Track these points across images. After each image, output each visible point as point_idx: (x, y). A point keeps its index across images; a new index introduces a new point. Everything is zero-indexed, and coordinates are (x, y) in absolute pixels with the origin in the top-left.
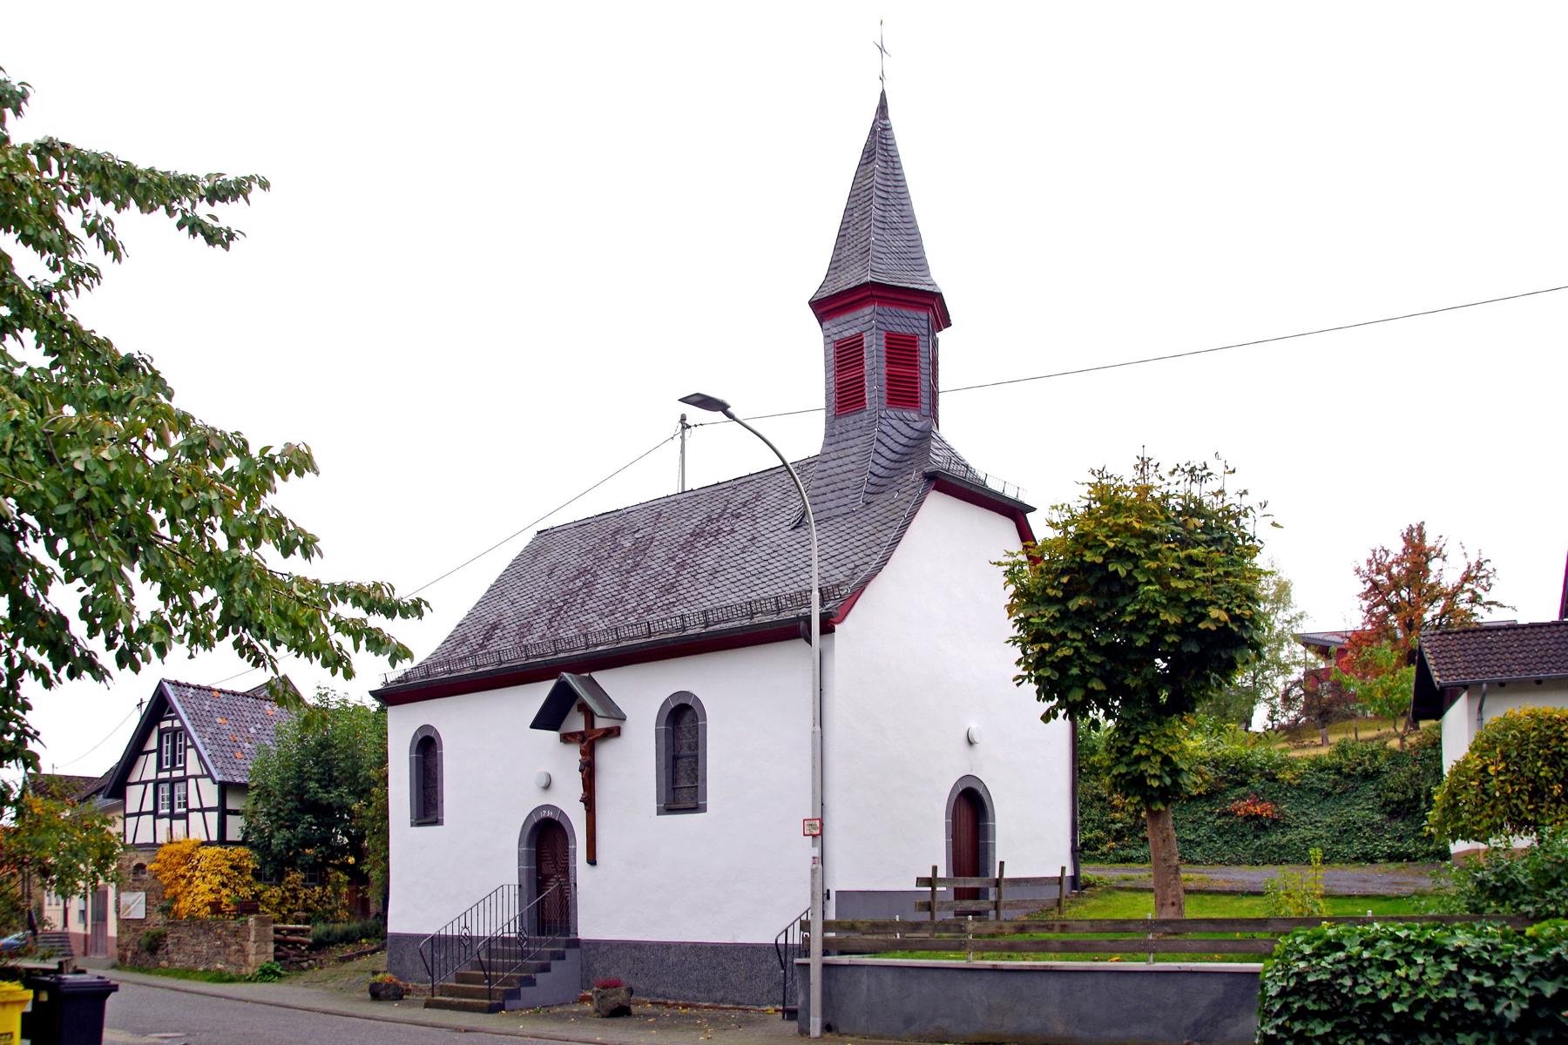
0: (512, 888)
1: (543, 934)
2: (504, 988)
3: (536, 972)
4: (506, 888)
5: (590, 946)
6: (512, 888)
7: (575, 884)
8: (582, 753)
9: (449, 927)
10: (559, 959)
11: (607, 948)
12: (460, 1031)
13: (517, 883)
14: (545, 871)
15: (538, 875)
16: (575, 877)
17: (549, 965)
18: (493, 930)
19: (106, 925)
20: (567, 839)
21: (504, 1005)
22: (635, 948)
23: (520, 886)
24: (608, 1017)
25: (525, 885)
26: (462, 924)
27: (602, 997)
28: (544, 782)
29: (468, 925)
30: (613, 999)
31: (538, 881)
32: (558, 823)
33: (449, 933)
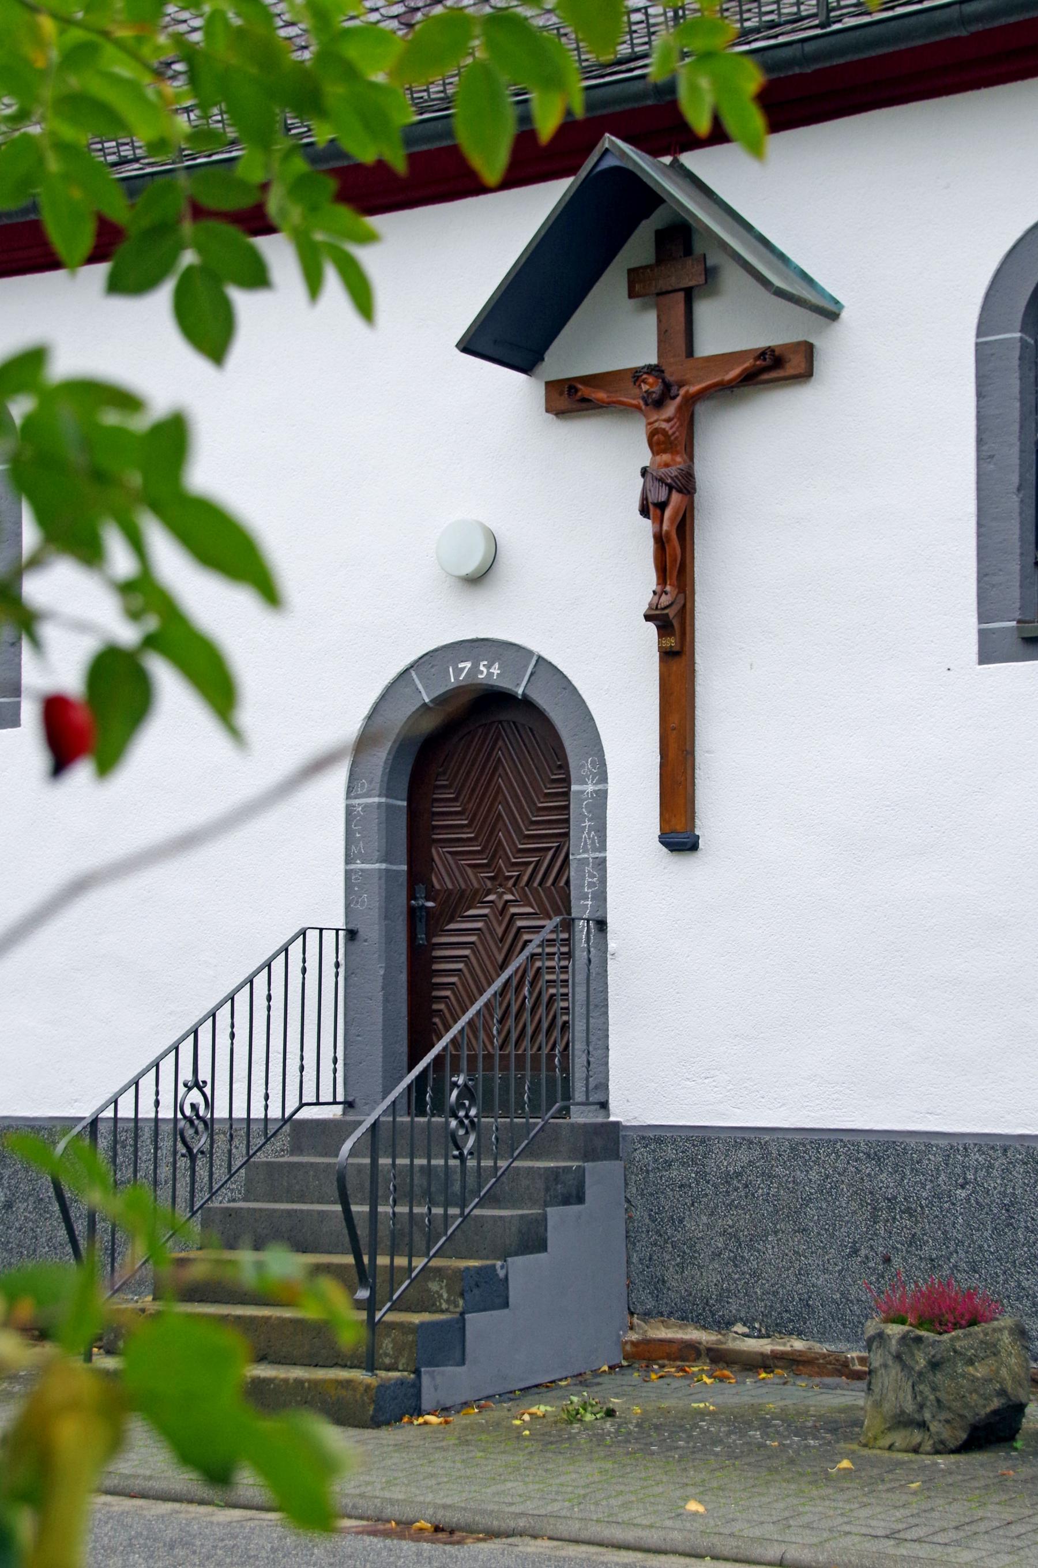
0: (329, 937)
1: (422, 1113)
2: (416, 1318)
3: (505, 1256)
4: (312, 936)
5: (670, 1153)
6: (329, 937)
7: (602, 925)
8: (658, 442)
9: (128, 1097)
10: (566, 1200)
11: (743, 1156)
12: (404, 1529)
13: (341, 924)
14: (442, 879)
15: (412, 895)
16: (601, 897)
17: (542, 1221)
18: (292, 1104)
19: (559, 1205)
20: (564, 766)
21: (416, 1387)
22: (876, 1158)
23: (352, 934)
24: (964, 1448)
25: (372, 932)
26: (186, 1074)
27: (935, 1365)
28: (471, 565)
29: (204, 1075)
30: (980, 1371)
31: (413, 914)
32: (527, 704)
33: (147, 1112)
